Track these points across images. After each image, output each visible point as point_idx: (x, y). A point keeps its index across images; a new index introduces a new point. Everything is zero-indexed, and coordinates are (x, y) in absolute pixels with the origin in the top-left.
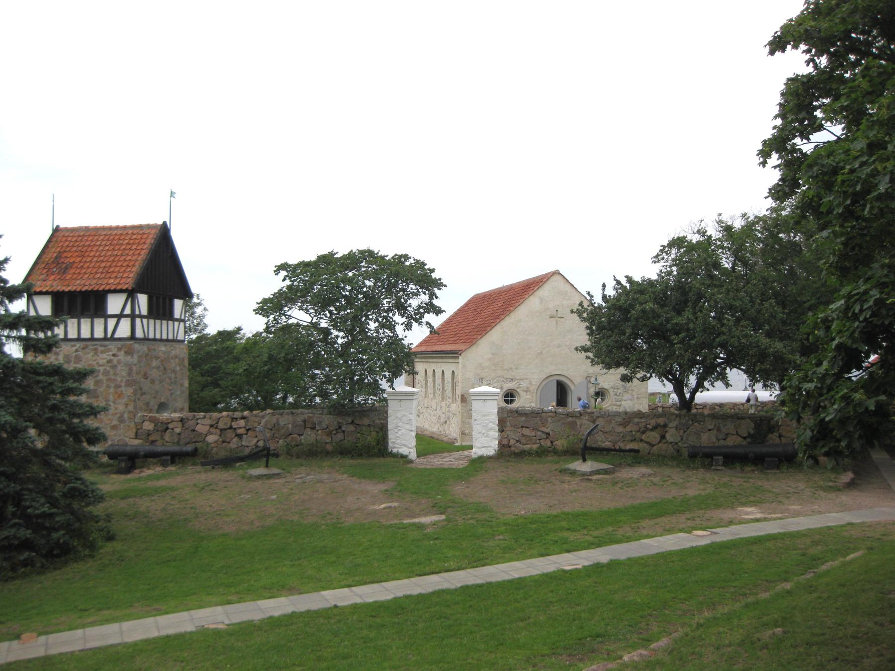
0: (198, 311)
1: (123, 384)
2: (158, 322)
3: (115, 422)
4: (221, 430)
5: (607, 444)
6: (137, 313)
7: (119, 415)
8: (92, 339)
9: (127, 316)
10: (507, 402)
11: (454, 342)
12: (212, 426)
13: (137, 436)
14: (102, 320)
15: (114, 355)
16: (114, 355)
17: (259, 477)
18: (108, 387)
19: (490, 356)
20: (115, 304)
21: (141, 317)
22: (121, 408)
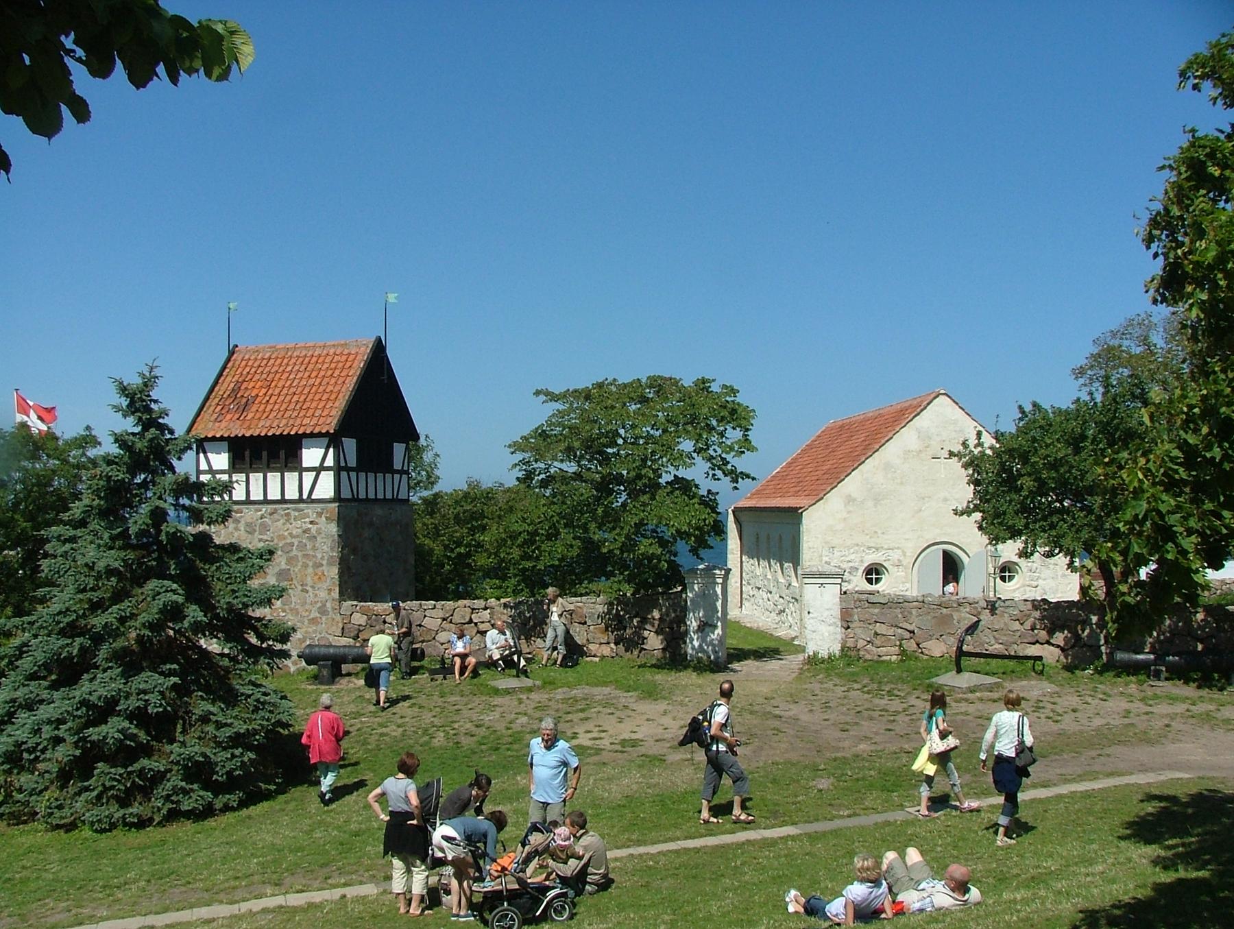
0: (427, 457)
1: (324, 562)
2: (371, 476)
3: (315, 614)
5: (997, 648)
6: (343, 464)
7: (319, 604)
8: (283, 501)
9: (328, 469)
10: (870, 581)
11: (796, 494)
12: (444, 619)
15: (311, 523)
16: (311, 523)
17: (508, 692)
18: (305, 566)
19: (845, 515)
20: (311, 456)
21: (348, 469)
22: (323, 594)
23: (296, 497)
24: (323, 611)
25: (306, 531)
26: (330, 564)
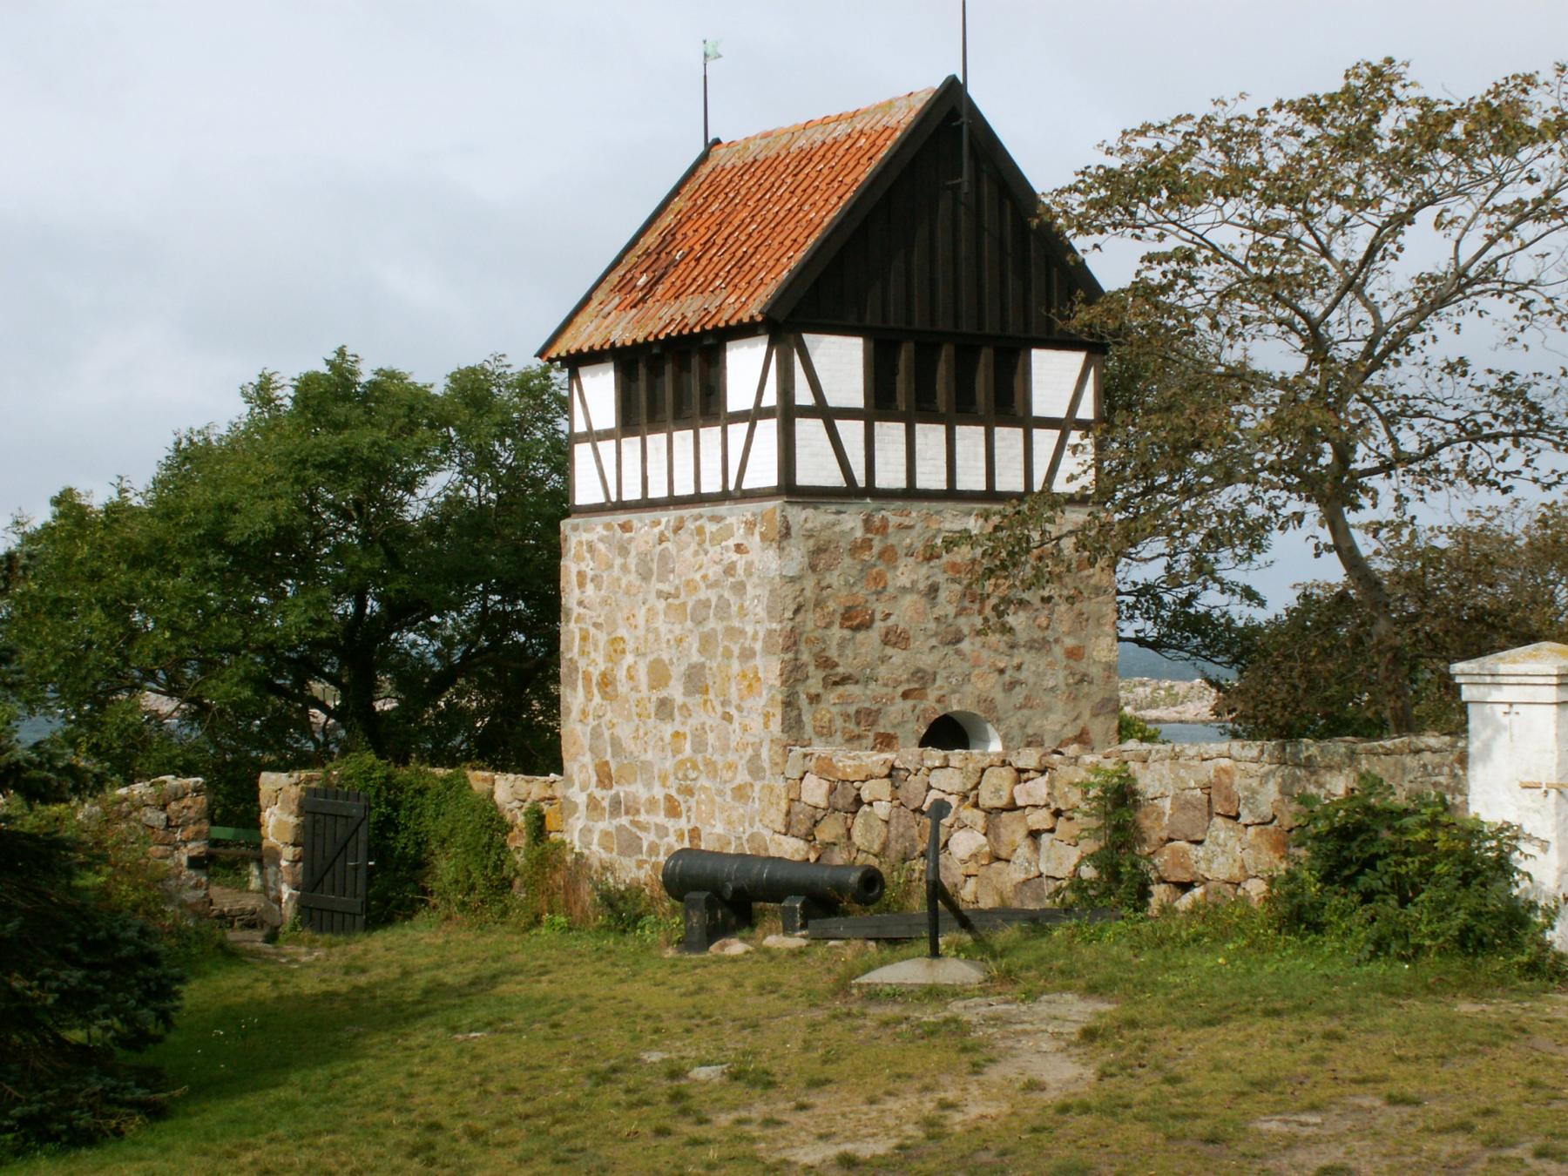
1: (758, 646)
3: (743, 777)
4: (990, 812)
6: (804, 397)
13: (788, 830)
14: (716, 431)
20: (746, 369)
22: (756, 723)
23: (1019, 486)
24: (755, 770)
25: (730, 570)
26: (768, 650)
